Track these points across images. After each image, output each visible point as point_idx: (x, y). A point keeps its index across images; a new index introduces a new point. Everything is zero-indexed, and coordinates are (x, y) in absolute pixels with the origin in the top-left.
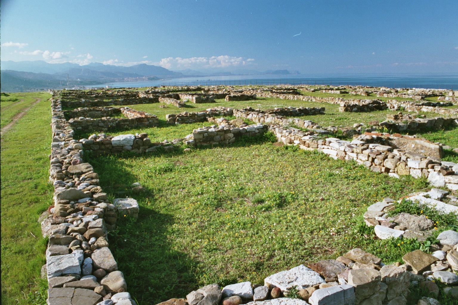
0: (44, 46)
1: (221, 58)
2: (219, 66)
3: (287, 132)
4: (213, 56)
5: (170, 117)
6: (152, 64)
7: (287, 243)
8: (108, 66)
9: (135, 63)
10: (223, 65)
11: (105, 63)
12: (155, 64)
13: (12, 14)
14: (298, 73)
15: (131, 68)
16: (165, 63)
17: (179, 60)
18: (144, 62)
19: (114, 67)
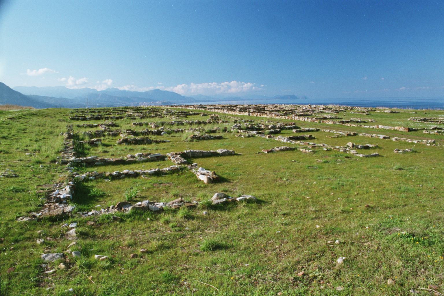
0: (53, 63)
1: (233, 83)
2: (229, 91)
3: (353, 220)
4: (227, 81)
5: (116, 173)
6: (165, 90)
7: (210, 230)
8: (124, 91)
9: (151, 88)
10: (233, 90)
11: (122, 89)
12: (169, 89)
13: (13, 13)
14: (306, 98)
15: (146, 93)
16: (179, 89)
17: (193, 86)
18: (158, 87)
19: (129, 92)
